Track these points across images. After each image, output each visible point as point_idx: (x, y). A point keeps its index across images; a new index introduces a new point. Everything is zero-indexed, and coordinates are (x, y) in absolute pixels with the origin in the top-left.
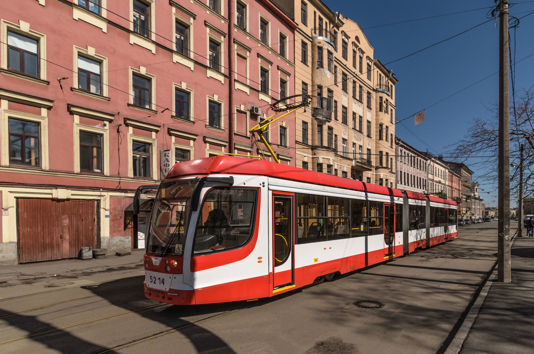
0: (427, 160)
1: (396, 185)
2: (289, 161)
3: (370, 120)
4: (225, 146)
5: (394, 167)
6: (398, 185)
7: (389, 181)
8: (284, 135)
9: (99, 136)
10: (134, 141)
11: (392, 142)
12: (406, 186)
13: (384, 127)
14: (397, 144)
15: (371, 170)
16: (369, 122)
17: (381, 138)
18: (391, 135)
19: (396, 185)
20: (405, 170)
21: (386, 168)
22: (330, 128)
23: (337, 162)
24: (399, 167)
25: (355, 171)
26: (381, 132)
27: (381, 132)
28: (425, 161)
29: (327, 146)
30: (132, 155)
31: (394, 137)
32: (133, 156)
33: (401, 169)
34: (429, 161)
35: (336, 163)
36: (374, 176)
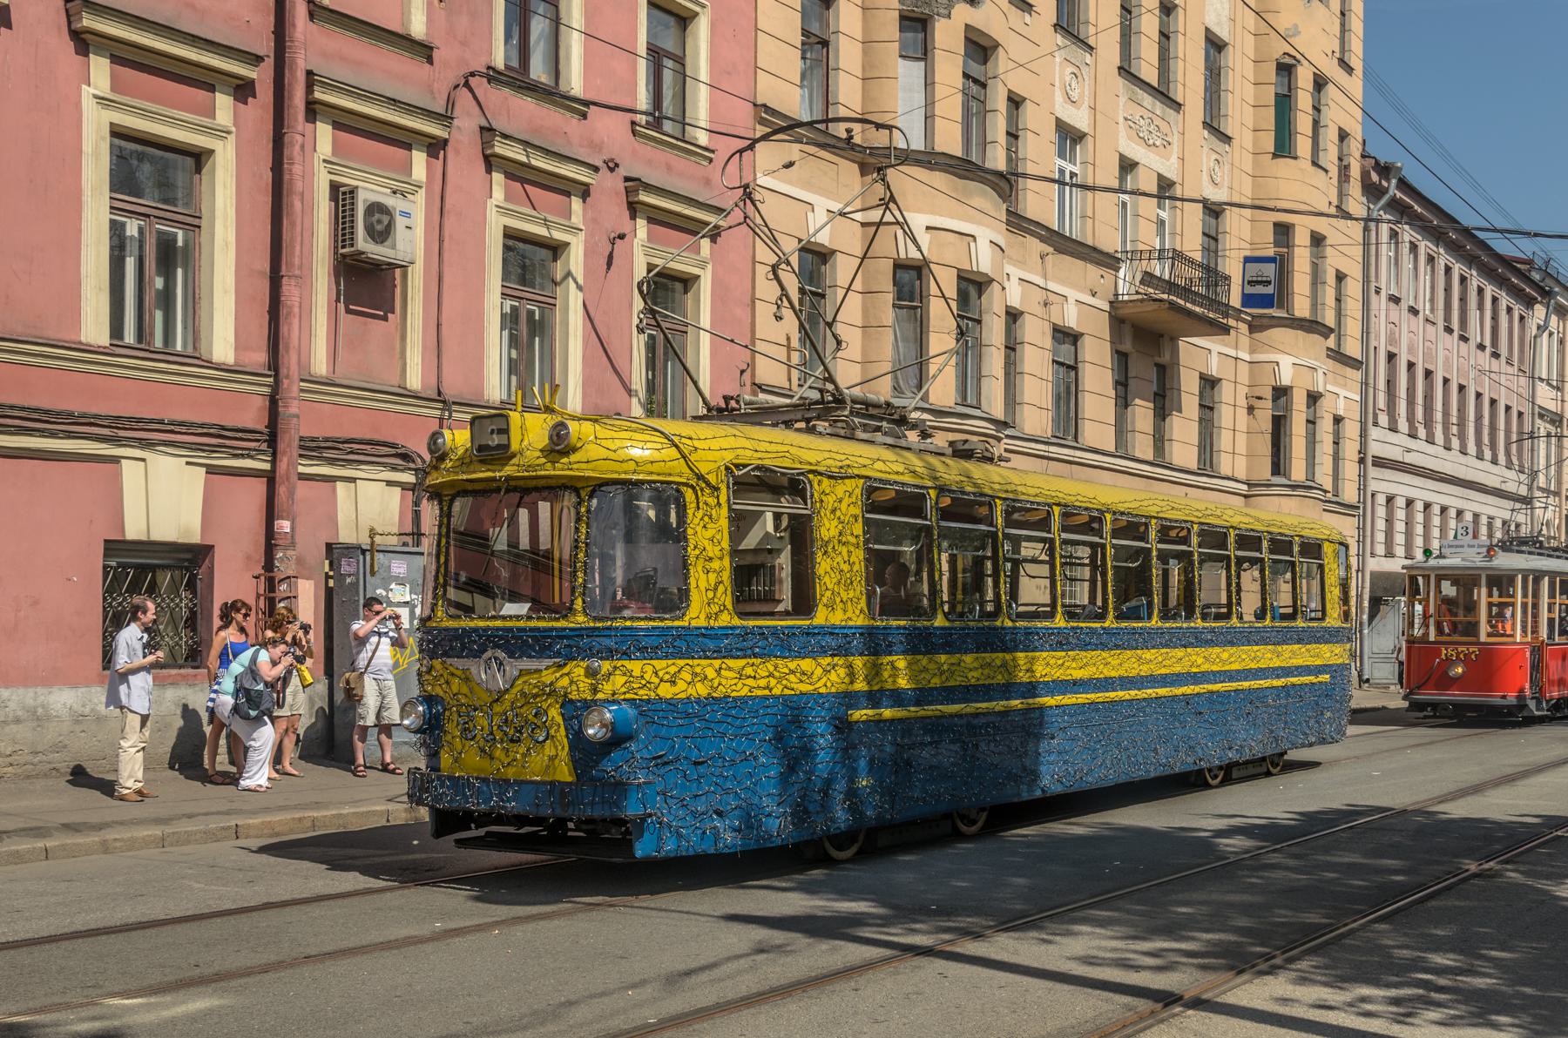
0: (1529, 303)
1: (1363, 434)
2: (585, 192)
3: (1223, 33)
4: (243, 90)
5: (1353, 328)
6: (1374, 433)
7: (1326, 408)
8: (680, 61)
9: (679, 286)
10: (117, 133)
11: (1344, 170)
12: (1420, 445)
13: (1304, 77)
14: (1372, 191)
15: (1226, 330)
16: (1215, 45)
17: (1284, 147)
18: (1343, 136)
19: (1363, 434)
20: (1411, 349)
21: (1311, 326)
22: (980, 48)
23: (1021, 263)
24: (1380, 327)
25: (1127, 329)
26: (1284, 104)
27: (1284, 104)
28: (1518, 309)
29: (957, 150)
30: (105, 216)
31: (1355, 148)
32: (112, 222)
33: (1392, 339)
34: (1540, 311)
35: (1015, 272)
36: (1244, 369)
